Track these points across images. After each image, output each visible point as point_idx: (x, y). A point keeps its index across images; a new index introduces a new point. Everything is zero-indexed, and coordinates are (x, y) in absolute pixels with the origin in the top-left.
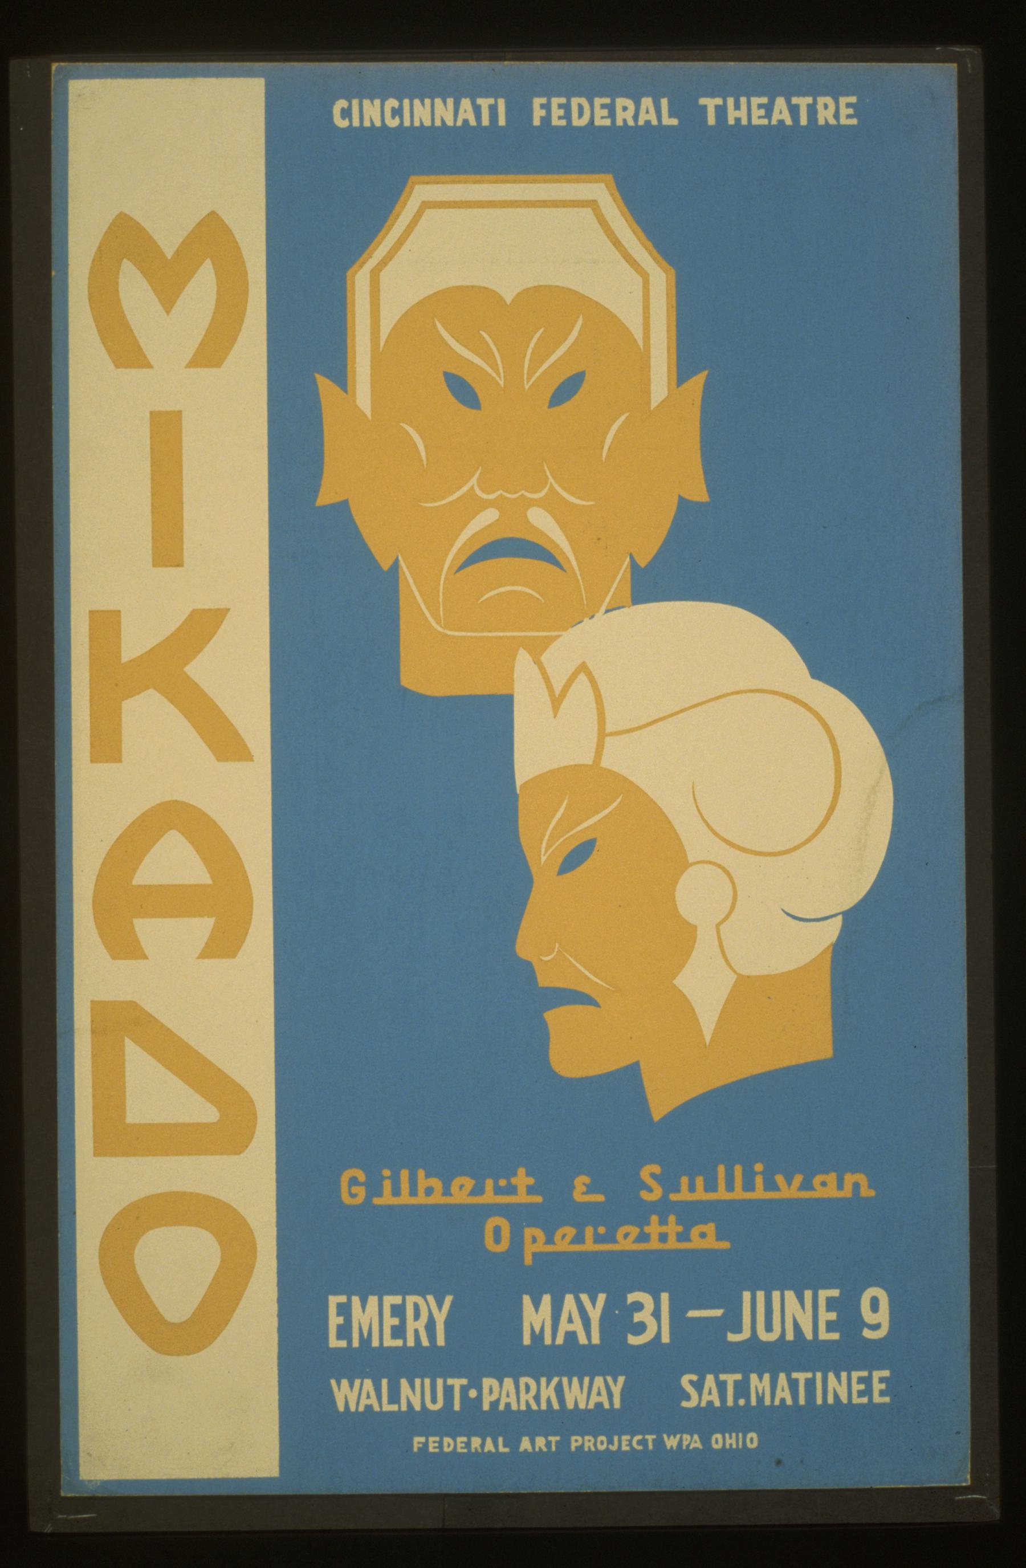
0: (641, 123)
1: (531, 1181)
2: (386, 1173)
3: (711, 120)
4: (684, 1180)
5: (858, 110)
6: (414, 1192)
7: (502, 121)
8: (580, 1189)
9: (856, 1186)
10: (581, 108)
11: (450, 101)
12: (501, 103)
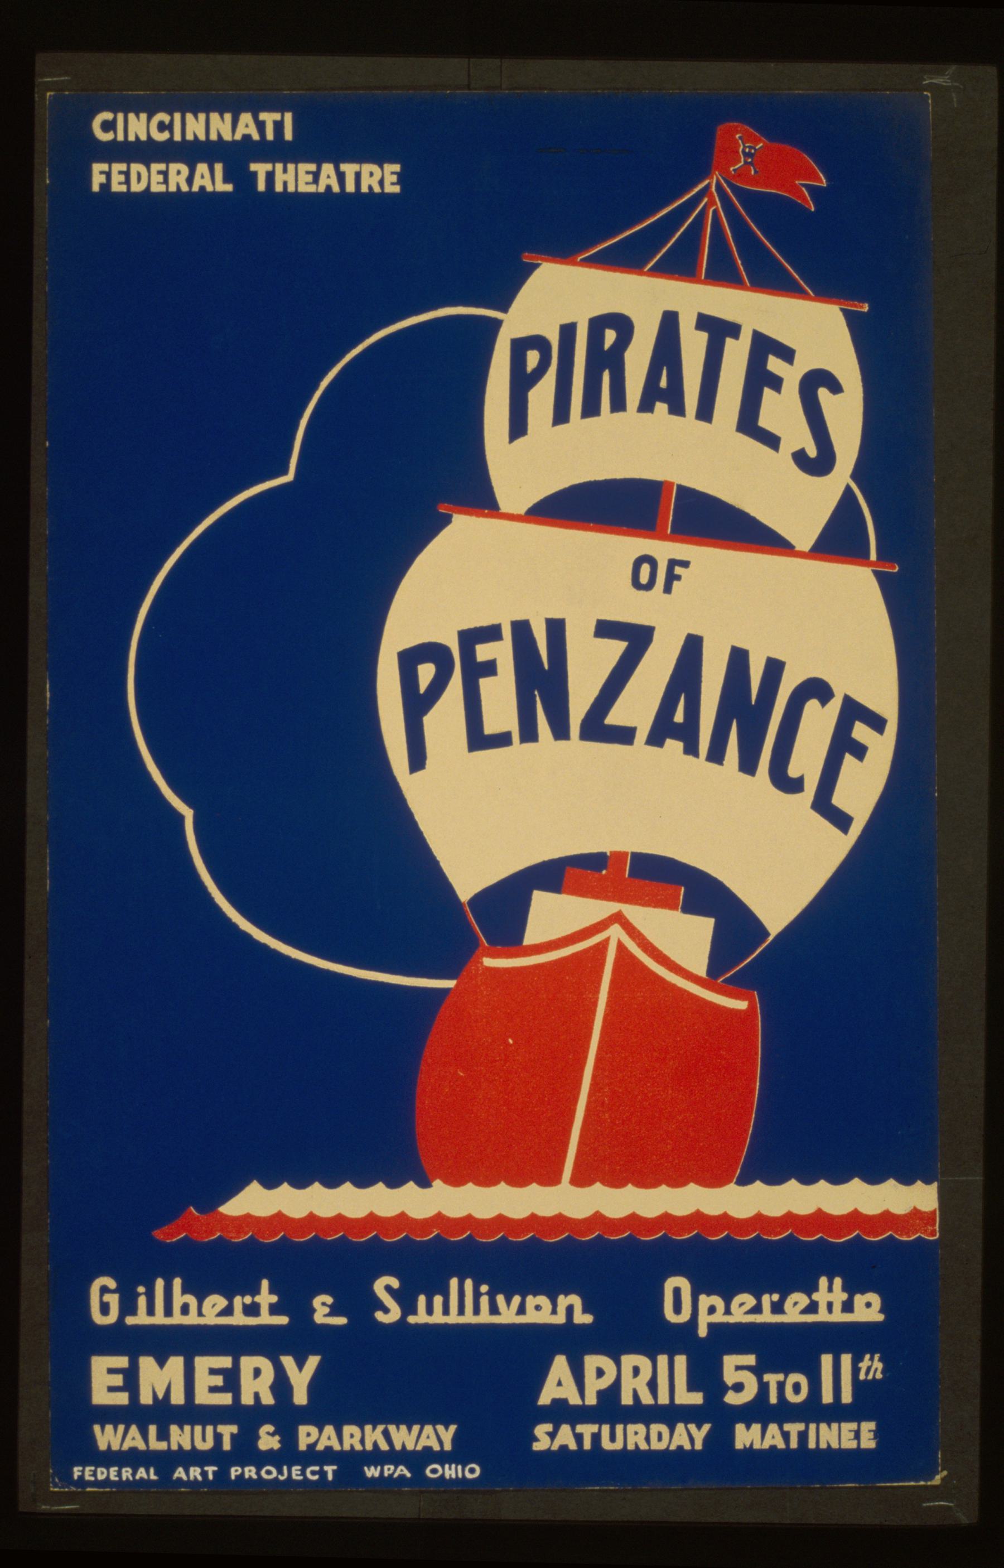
0: (195, 188)
1: (274, 1299)
2: (141, 1289)
3: (261, 186)
4: (422, 1300)
5: (402, 179)
6: (168, 1312)
7: (288, 136)
8: (322, 1309)
9: (570, 1310)
10: (139, 175)
11: (228, 117)
12: (288, 117)
